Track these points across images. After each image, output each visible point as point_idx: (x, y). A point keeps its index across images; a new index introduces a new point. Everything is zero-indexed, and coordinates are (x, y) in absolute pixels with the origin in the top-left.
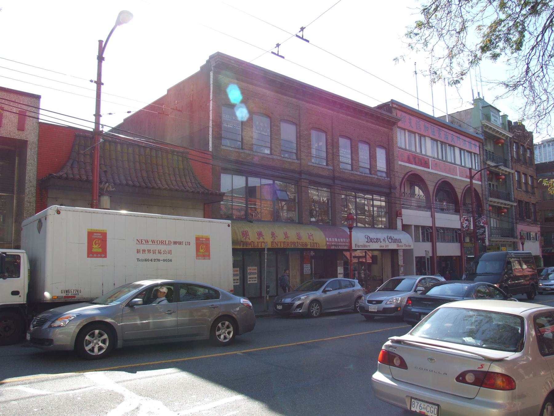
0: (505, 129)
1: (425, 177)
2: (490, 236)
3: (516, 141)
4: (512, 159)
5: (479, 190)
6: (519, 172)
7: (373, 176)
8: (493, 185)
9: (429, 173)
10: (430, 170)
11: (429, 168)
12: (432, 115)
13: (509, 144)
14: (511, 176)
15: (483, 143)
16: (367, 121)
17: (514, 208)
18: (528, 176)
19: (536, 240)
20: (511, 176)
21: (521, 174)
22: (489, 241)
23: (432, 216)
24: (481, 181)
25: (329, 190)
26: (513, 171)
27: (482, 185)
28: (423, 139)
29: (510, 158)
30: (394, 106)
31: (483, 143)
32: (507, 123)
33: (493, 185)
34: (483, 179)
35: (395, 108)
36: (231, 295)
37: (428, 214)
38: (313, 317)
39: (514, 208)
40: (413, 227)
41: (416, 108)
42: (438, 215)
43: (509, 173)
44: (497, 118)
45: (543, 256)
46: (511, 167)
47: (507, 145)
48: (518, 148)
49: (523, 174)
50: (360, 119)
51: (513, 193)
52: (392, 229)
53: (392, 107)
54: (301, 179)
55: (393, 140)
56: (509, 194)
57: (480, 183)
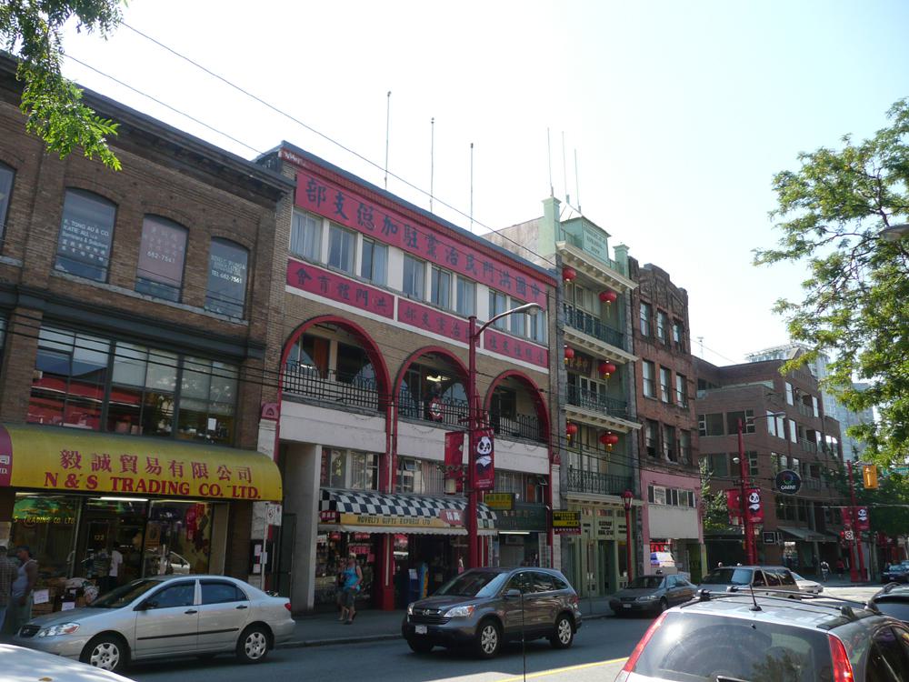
0: (622, 273)
1: (376, 336)
2: (562, 490)
3: (646, 300)
4: (633, 335)
5: (541, 384)
6: (651, 363)
7: (188, 308)
8: (593, 385)
9: (389, 327)
10: (394, 322)
11: (391, 317)
12: (383, 188)
13: (629, 303)
14: (631, 367)
15: (557, 289)
16: (182, 171)
17: (635, 435)
18: (674, 373)
19: (691, 505)
20: (631, 367)
21: (657, 366)
22: (563, 499)
23: (387, 430)
24: (548, 367)
25: (237, 370)
26: (635, 359)
27: (549, 376)
28: (499, 299)
29: (630, 332)
30: (288, 156)
31: (557, 289)
32: (626, 262)
33: (593, 385)
34: (553, 363)
35: (291, 162)
36: (689, 583)
37: (378, 423)
38: (248, 662)
39: (635, 435)
40: (319, 452)
41: (382, 187)
42: (404, 428)
43: (627, 361)
44: (600, 246)
45: (706, 538)
46: (630, 348)
47: (625, 304)
48: (651, 315)
49: (662, 367)
50: (154, 159)
51: (633, 403)
52: (233, 446)
53: (283, 159)
54: (16, 305)
55: (272, 233)
56: (626, 404)
57: (546, 371)
